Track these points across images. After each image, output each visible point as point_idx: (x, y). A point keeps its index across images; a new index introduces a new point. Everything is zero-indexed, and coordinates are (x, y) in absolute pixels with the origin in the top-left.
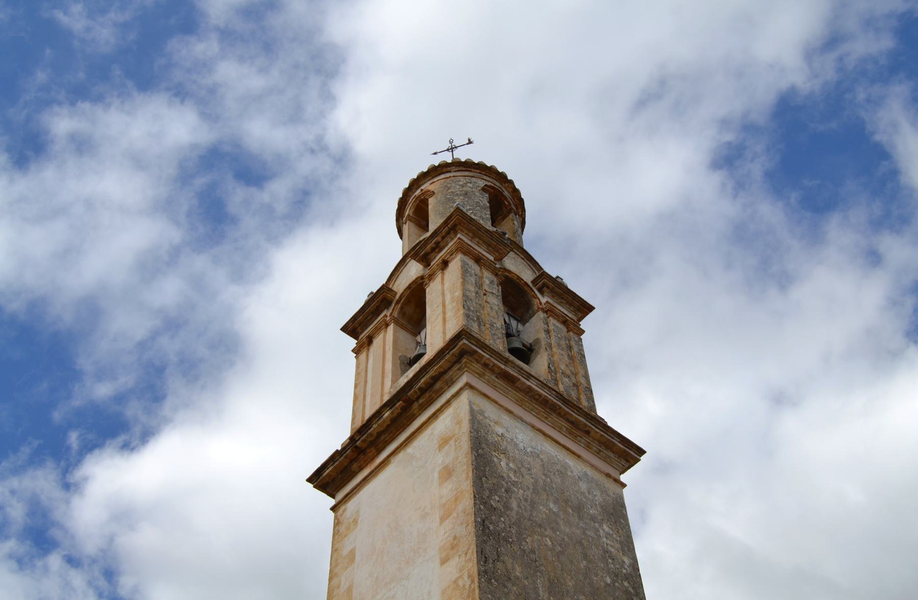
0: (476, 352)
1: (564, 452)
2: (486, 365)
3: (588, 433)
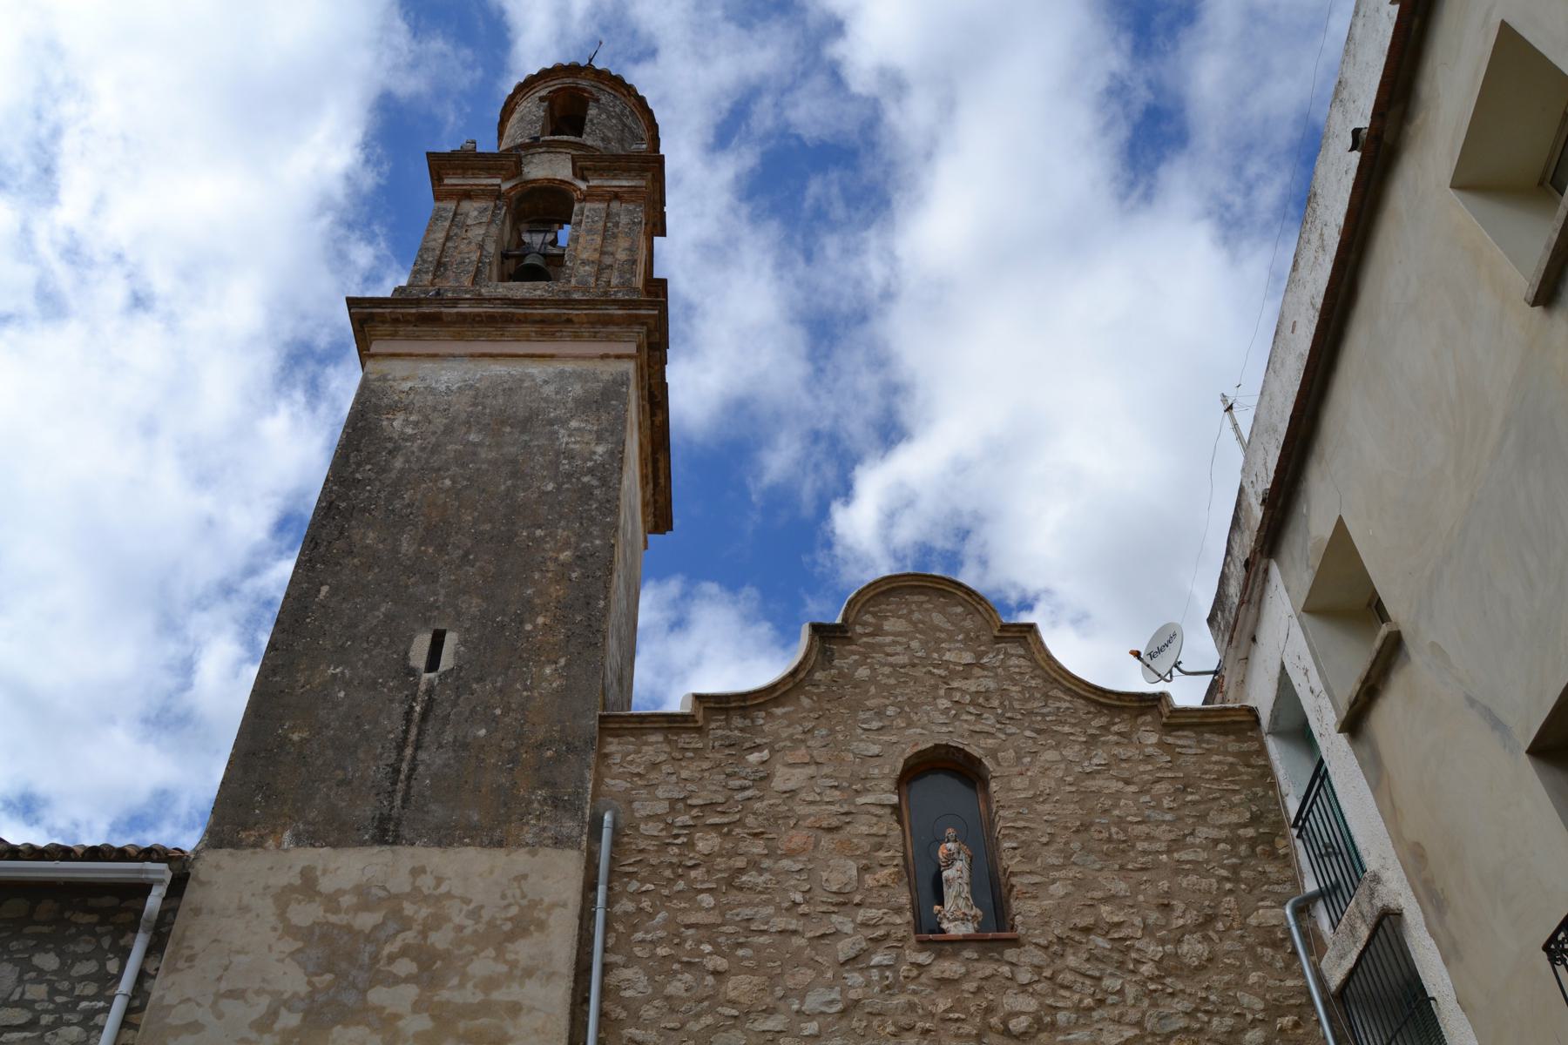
1: (527, 362)
2: (396, 321)
3: (569, 321)
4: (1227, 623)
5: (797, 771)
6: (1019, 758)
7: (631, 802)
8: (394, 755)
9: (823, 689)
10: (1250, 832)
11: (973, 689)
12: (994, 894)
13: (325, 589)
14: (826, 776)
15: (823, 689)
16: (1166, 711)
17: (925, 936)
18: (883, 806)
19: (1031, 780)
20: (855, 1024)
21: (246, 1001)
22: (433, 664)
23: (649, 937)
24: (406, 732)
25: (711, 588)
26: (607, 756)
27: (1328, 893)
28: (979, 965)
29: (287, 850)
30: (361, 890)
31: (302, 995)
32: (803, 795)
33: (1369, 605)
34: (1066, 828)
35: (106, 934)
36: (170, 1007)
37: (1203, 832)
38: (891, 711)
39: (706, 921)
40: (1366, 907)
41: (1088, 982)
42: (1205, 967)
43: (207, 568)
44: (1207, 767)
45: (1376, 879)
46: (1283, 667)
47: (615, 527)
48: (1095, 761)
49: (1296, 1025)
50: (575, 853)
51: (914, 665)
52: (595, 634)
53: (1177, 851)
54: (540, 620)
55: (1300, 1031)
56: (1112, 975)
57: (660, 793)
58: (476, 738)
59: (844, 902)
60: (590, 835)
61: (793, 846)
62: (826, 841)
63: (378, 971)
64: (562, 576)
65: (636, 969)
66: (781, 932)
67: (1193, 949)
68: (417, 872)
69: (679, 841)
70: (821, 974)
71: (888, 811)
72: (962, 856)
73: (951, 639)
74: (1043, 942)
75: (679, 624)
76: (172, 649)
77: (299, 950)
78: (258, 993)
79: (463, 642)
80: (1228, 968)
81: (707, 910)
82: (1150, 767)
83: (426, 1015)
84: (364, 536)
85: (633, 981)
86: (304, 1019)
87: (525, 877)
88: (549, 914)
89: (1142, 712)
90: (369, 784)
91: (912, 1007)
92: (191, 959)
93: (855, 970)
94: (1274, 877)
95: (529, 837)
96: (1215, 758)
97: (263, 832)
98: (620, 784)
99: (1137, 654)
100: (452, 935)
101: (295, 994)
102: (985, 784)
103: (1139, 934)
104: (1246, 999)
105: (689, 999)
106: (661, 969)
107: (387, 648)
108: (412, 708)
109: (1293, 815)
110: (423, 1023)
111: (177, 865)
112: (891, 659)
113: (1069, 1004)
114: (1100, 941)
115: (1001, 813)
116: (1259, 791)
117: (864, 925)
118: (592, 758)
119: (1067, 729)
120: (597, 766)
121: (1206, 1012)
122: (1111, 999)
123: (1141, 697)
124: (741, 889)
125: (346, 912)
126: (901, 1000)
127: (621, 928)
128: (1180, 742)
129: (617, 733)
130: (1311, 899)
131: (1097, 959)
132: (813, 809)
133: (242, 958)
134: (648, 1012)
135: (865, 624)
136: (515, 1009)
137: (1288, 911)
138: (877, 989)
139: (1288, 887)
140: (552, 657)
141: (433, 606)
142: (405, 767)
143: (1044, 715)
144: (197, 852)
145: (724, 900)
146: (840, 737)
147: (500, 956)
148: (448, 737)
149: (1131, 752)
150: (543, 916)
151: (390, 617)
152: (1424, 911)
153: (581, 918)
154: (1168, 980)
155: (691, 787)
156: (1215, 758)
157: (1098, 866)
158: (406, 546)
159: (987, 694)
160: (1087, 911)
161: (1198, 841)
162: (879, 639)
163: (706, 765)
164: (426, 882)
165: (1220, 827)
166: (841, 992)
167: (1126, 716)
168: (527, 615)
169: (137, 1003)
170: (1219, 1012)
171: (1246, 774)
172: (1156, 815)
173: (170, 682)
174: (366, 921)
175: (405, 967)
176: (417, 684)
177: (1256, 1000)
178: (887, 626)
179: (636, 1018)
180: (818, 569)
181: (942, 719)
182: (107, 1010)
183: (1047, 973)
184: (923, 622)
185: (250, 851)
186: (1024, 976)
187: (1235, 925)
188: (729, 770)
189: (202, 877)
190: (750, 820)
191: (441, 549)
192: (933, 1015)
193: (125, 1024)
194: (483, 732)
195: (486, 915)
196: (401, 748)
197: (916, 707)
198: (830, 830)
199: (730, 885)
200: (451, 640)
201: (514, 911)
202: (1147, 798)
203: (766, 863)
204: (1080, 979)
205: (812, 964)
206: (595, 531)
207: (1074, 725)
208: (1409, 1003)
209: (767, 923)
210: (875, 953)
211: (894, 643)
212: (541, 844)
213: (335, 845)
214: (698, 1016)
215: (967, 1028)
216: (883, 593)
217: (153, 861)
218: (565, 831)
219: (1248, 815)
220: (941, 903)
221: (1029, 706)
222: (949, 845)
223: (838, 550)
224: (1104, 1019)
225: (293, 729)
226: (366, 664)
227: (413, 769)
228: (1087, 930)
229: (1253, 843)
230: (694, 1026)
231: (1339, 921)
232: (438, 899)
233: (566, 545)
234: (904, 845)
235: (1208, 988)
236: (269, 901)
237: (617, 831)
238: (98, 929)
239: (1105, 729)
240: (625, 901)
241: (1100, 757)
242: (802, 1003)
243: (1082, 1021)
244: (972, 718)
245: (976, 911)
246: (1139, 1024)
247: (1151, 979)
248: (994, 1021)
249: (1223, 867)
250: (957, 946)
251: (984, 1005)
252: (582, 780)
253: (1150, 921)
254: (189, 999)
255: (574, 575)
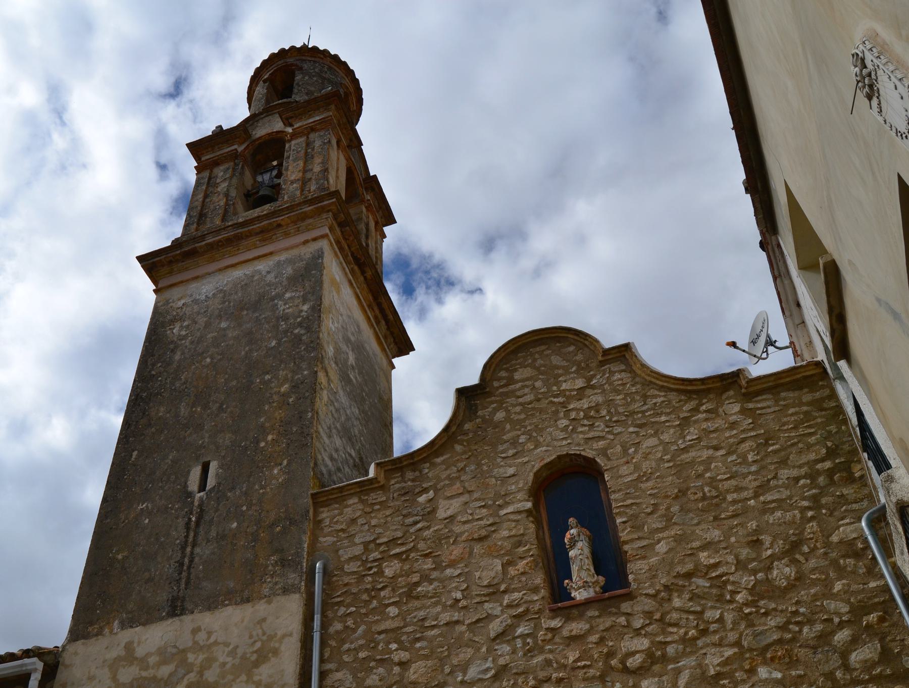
0: (153, 263)
2: (170, 262)
3: (279, 226)
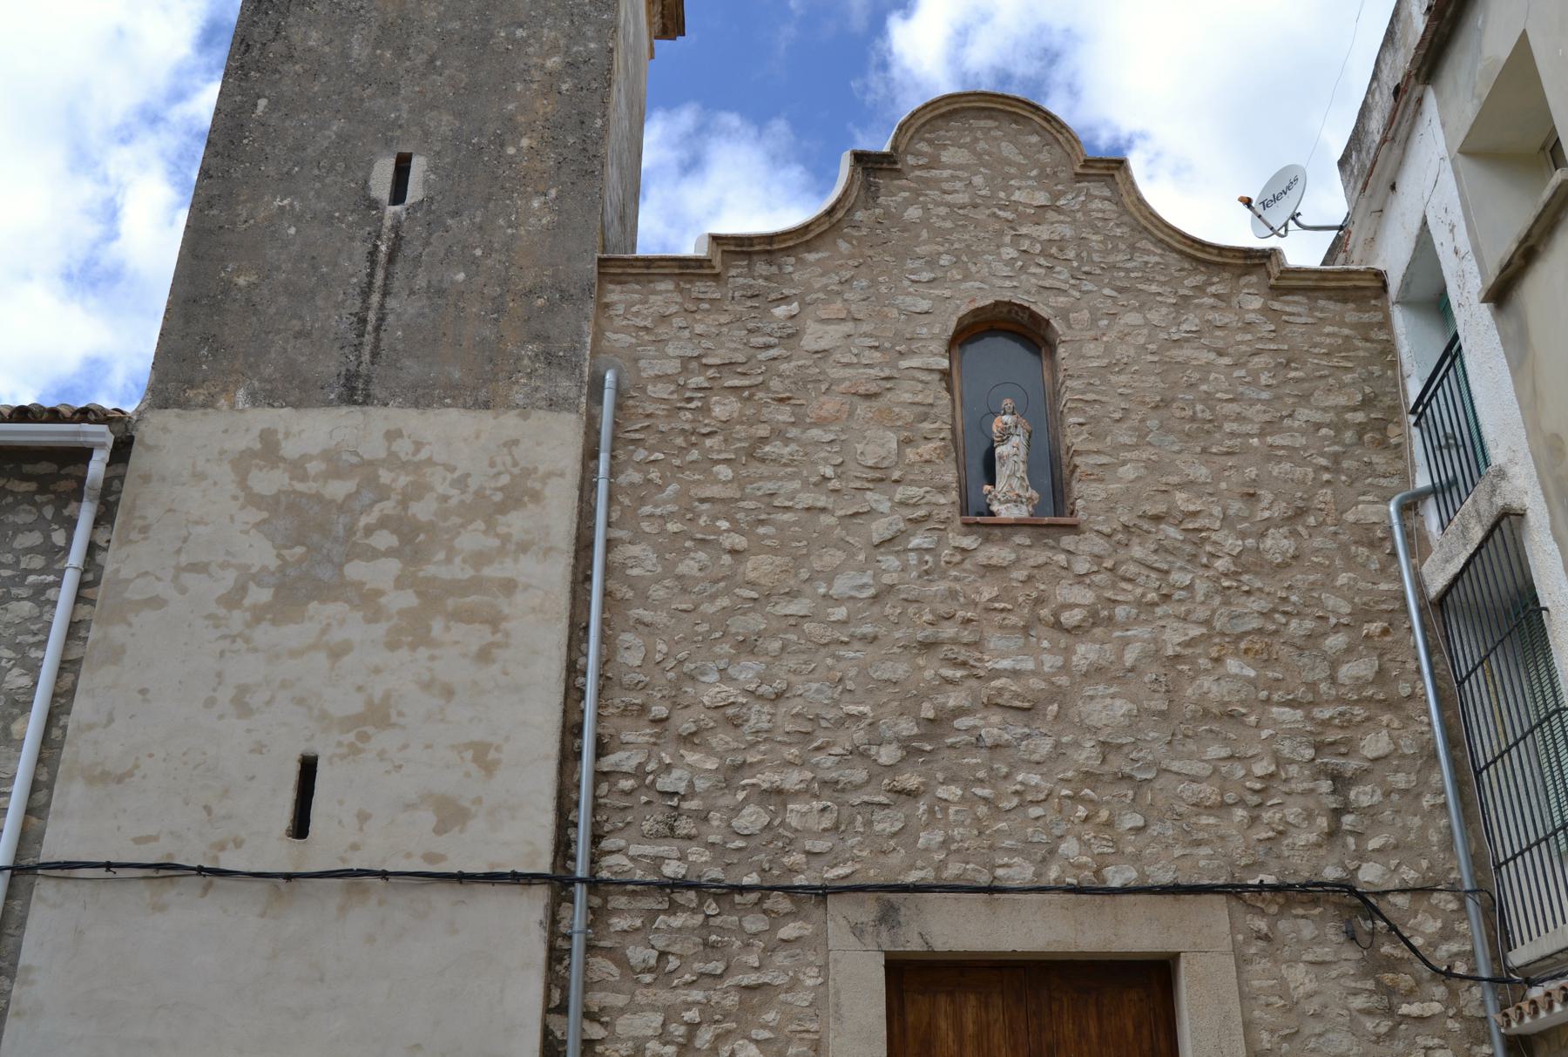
4: (1363, 166)
5: (831, 328)
6: (1094, 321)
7: (636, 360)
8: (358, 303)
9: (864, 231)
10: (1360, 417)
11: (1045, 237)
12: (1054, 478)
13: (262, 103)
14: (865, 335)
15: (864, 231)
16: (1275, 271)
17: (972, 519)
18: (931, 371)
19: (1107, 345)
20: (888, 610)
21: (210, 575)
22: (398, 195)
23: (658, 511)
24: (371, 275)
25: (732, 120)
26: (607, 306)
27: (1443, 491)
28: (1032, 552)
29: (242, 411)
30: (329, 456)
31: (272, 568)
32: (837, 356)
33: (1543, 148)
34: (1144, 403)
35: (47, 503)
36: (128, 581)
37: (1304, 414)
38: (945, 260)
39: (723, 495)
40: (1483, 506)
41: (1154, 575)
42: (1288, 565)
43: (119, 96)
44: (1318, 339)
45: (1501, 474)
46: (1425, 223)
47: (614, 27)
48: (1185, 327)
49: (1385, 632)
50: (574, 416)
51: (975, 206)
52: (594, 166)
53: (1271, 434)
54: (525, 142)
55: (1388, 639)
56: (1182, 569)
57: (671, 350)
58: (453, 283)
59: (880, 478)
60: (590, 396)
61: (823, 413)
62: (862, 408)
63: (355, 544)
64: (550, 89)
65: (643, 546)
66: (808, 509)
67: (1277, 544)
68: (392, 435)
69: (692, 405)
70: (852, 556)
71: (936, 377)
72: (1020, 431)
73: (1023, 175)
74: (1107, 530)
75: (692, 165)
76: (87, 190)
77: (264, 521)
78: (224, 566)
79: (433, 169)
80: (1316, 567)
81: (725, 483)
82: (1249, 337)
83: (410, 591)
84: (306, 37)
85: (641, 558)
86: (276, 595)
87: (516, 442)
88: (545, 484)
89: (1247, 270)
90: (332, 336)
91: (953, 594)
92: (144, 530)
93: (891, 553)
94: (1381, 469)
95: (519, 398)
96: (1328, 329)
97: (213, 390)
98: (624, 339)
99: (1248, 202)
100: (435, 506)
101: (264, 568)
102: (1052, 348)
103: (1217, 525)
104: (1331, 601)
105: (703, 579)
106: (672, 547)
107: (343, 175)
108: (376, 247)
109: (1413, 400)
110: (408, 599)
111: (119, 427)
112: (948, 198)
113: (1130, 598)
114: (1173, 532)
115: (1068, 383)
116: (1376, 370)
117: (903, 504)
118: (590, 307)
119: (1154, 288)
120: (597, 318)
121: (1285, 613)
122: (1178, 595)
123: (1247, 253)
124: (763, 460)
125: (315, 480)
126: (941, 586)
127: (627, 501)
128: (1288, 309)
129: (619, 280)
130: (1422, 495)
131: (1166, 551)
132: (849, 372)
133: (200, 529)
134: (657, 592)
135: (918, 154)
136: (509, 586)
137: (1392, 508)
138: (914, 574)
139: (1396, 481)
140: (541, 188)
141: (395, 124)
142: (372, 317)
143: (1128, 271)
144: (139, 412)
145: (744, 472)
146: (883, 289)
147: (490, 528)
148: (421, 282)
149: (1228, 318)
150: (538, 486)
151: (343, 138)
152: (1551, 512)
153: (581, 489)
154: (1245, 578)
155: (706, 343)
156: (1328, 329)
157: (1176, 448)
158: (359, 49)
159: (1062, 243)
160: (1159, 497)
161: (1296, 424)
162: (934, 173)
163: (724, 319)
164: (403, 447)
165: (1325, 410)
166: (874, 576)
167: (1226, 275)
168: (508, 137)
169: (90, 577)
170: (1298, 614)
171: (1363, 349)
172: (1251, 393)
173: (93, 230)
174: (338, 489)
175: (384, 540)
176: (381, 219)
177: (1343, 603)
178: (945, 157)
179: (644, 599)
180: (869, 98)
181: (1006, 271)
182: (58, 584)
183: (1109, 564)
184: (989, 154)
185: (199, 412)
186: (1081, 566)
187: (1329, 520)
188: (751, 325)
189: (149, 441)
190: (775, 383)
191: (401, 53)
192: (976, 604)
193: (79, 599)
194: (461, 276)
195: (473, 484)
196: (366, 293)
197: (974, 255)
198: (868, 396)
199: (751, 456)
200: (418, 166)
201: (505, 480)
202: (1242, 373)
203: (793, 432)
204: (1145, 572)
205: (842, 544)
206: (590, 31)
207: (1163, 284)
208: (1517, 615)
209: (792, 499)
210: (914, 535)
211: (954, 178)
212: (535, 407)
213: (297, 405)
214: (713, 598)
215: (1013, 619)
216: (942, 116)
217: (90, 422)
218: (561, 391)
219: (1359, 397)
220: (992, 482)
221: (1111, 259)
222: (1005, 418)
223: (895, 72)
224: (1169, 616)
225: (238, 271)
226: (318, 195)
227: (381, 319)
228: (1157, 519)
229: (1361, 429)
230: (708, 608)
231: (1450, 521)
232: (419, 466)
233: (555, 49)
234: (953, 417)
235: (1290, 588)
236: (227, 467)
237: (619, 392)
238: (38, 498)
239: (1200, 289)
240: (630, 471)
241: (1191, 322)
242: (830, 586)
243: (1143, 617)
244: (1043, 271)
245: (1032, 493)
246: (1207, 622)
247: (1226, 575)
248: (1045, 612)
249: (1322, 455)
250: (1008, 530)
251: (1034, 595)
252: (579, 333)
253: (1231, 512)
254: (146, 573)
255: (564, 87)
